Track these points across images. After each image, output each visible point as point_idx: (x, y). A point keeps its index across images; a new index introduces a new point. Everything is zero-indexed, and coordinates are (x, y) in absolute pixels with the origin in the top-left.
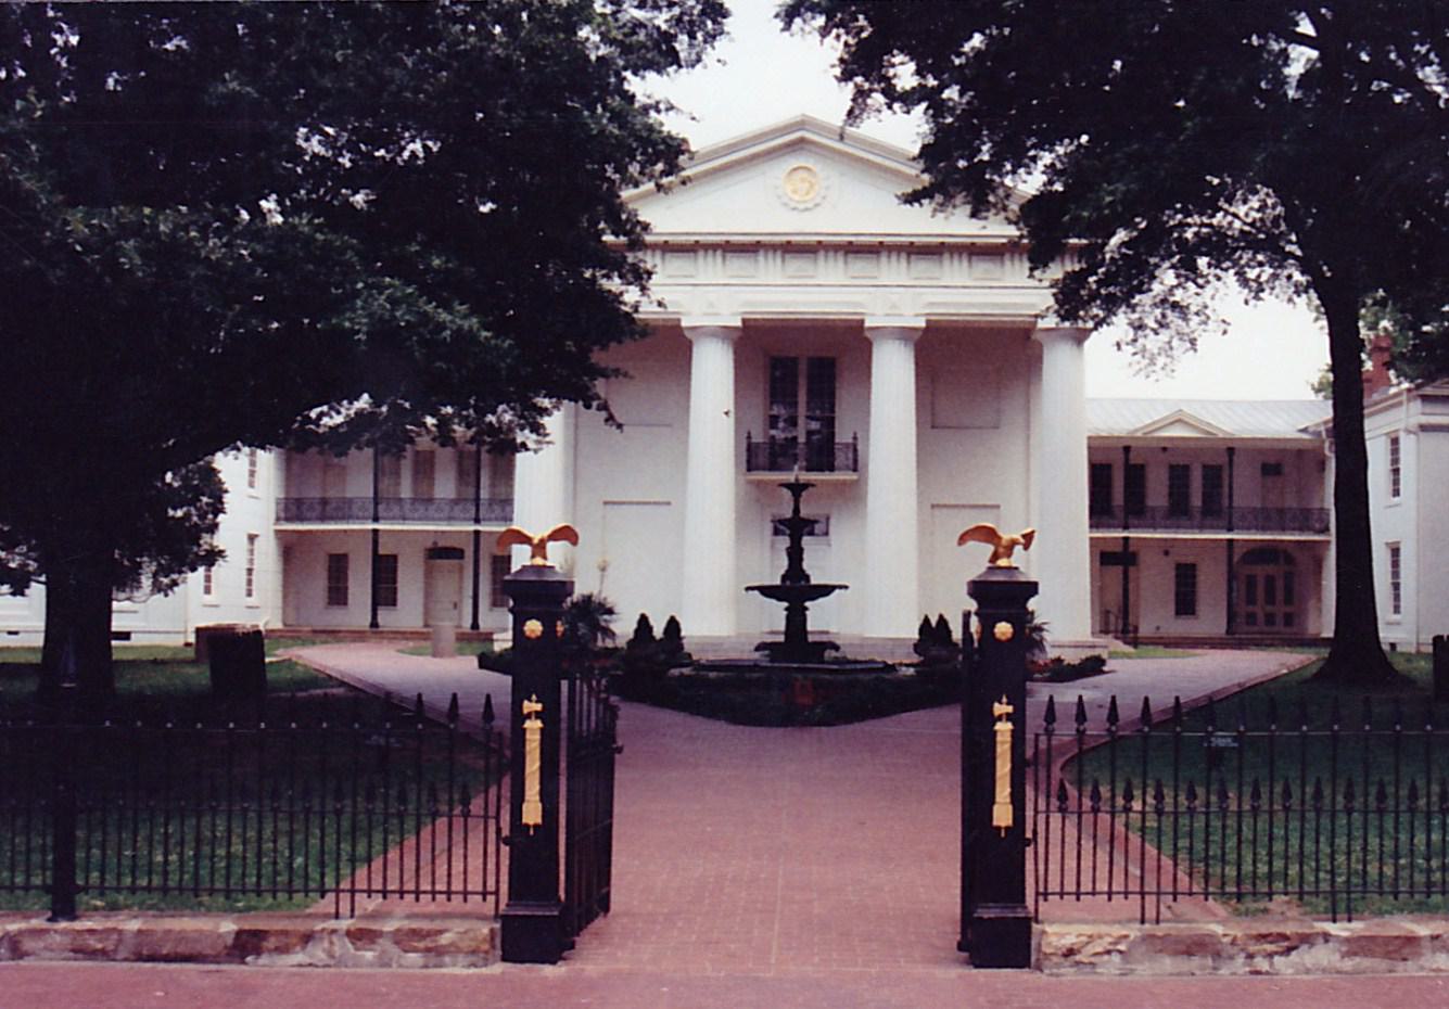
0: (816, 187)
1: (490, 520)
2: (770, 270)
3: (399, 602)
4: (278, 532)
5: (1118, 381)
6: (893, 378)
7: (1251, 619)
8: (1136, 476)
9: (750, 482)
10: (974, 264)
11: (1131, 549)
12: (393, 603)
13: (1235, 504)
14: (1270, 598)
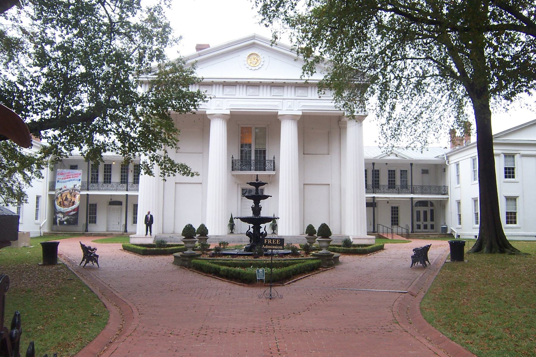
0: (259, 61)
1: (132, 190)
2: (240, 92)
3: (97, 222)
4: (49, 195)
5: (370, 137)
6: (288, 134)
7: (419, 227)
8: (376, 174)
9: (233, 175)
10: (272, 90)
11: (375, 201)
12: (95, 222)
13: (413, 184)
14: (425, 219)
